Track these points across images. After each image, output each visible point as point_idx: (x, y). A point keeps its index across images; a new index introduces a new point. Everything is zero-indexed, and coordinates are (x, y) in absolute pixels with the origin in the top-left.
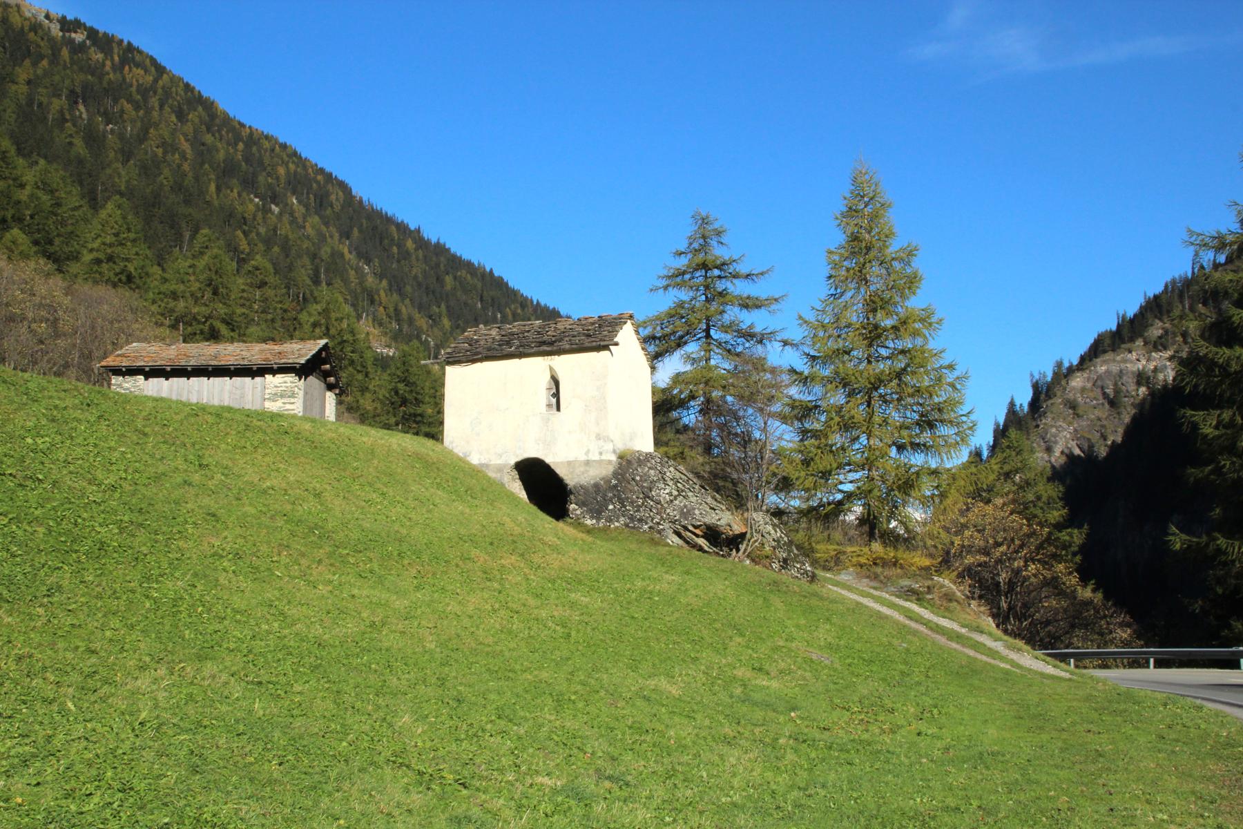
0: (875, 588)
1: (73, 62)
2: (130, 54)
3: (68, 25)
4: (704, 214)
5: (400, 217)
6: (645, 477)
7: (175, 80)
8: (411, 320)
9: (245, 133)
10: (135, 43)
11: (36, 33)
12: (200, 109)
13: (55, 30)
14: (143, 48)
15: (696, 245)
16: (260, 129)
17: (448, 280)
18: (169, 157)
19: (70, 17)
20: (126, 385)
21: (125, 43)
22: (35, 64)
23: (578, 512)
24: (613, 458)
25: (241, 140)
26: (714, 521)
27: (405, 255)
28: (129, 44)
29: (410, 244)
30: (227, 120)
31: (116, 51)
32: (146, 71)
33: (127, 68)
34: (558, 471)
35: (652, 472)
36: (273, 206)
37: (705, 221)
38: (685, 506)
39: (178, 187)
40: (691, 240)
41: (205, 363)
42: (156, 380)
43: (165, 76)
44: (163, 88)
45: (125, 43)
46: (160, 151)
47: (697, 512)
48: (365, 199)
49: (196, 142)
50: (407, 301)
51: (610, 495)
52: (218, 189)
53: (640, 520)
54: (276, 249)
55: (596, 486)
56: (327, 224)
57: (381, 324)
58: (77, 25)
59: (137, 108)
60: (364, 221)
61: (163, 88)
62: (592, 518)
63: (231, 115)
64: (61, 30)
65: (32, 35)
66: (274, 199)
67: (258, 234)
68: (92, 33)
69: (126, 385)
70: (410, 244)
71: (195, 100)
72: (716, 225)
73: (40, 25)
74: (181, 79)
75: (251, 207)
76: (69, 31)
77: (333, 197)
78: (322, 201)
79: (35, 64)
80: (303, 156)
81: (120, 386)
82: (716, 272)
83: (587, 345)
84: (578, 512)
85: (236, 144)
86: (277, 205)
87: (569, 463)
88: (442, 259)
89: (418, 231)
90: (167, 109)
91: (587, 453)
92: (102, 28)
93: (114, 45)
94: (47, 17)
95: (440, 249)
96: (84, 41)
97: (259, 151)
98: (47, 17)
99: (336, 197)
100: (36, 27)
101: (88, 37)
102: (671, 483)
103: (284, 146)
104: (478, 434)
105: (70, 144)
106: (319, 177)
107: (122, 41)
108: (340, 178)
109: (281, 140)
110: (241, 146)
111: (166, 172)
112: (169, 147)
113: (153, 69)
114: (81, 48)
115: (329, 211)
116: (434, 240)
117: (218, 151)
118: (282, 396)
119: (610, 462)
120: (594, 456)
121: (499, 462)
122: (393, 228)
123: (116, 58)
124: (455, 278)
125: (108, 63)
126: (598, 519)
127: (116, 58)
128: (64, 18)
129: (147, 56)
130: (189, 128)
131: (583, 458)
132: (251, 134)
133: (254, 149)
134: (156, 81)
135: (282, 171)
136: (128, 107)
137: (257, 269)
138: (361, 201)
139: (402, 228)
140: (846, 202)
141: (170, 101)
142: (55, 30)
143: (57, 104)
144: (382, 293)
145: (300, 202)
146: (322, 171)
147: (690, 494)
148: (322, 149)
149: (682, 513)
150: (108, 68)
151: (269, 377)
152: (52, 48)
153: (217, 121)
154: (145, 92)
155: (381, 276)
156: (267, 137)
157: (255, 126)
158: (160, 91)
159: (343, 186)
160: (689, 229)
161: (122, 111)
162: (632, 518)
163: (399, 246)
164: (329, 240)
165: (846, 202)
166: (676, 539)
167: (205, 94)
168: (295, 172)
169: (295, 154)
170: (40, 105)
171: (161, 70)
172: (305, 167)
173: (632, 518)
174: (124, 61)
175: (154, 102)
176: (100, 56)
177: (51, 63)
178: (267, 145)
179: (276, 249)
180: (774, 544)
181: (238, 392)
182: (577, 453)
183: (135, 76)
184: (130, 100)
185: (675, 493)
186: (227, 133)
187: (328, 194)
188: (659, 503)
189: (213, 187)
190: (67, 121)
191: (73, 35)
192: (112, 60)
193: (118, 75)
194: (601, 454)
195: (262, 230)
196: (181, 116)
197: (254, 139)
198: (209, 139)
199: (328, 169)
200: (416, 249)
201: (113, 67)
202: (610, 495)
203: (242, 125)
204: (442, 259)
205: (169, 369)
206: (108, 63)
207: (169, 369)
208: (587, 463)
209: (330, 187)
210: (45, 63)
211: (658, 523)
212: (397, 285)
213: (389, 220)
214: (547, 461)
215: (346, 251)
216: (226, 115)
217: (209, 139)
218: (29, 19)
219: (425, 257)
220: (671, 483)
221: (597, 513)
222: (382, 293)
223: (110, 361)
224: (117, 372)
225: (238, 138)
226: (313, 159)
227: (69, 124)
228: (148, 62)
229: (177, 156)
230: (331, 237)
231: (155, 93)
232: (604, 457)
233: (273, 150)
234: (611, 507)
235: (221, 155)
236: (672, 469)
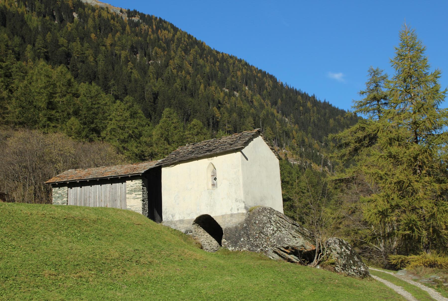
0: (415, 280)
1: (132, 32)
2: (161, 24)
3: (131, 14)
4: (375, 69)
5: (303, 91)
6: (261, 221)
7: (184, 34)
8: (310, 146)
9: (220, 56)
10: (163, 18)
11: (114, 20)
12: (196, 47)
13: (125, 17)
14: (167, 20)
15: (372, 87)
16: (228, 53)
17: (331, 121)
18: (179, 73)
19: (132, 10)
20: (59, 192)
21: (158, 19)
22: (114, 36)
23: (226, 243)
24: (245, 211)
25: (218, 60)
26: (294, 244)
27: (307, 110)
28: (160, 19)
29: (309, 104)
30: (210, 51)
31: (154, 23)
32: (169, 31)
33: (160, 31)
34: (217, 221)
35: (265, 218)
36: (235, 93)
37: (375, 73)
38: (280, 236)
39: (184, 88)
40: (369, 84)
41: (95, 177)
42: (86, 187)
43: (178, 33)
44: (178, 39)
45: (158, 19)
46: (175, 71)
47: (286, 239)
48: (284, 83)
49: (194, 64)
50: (310, 135)
51: (242, 232)
52: (205, 87)
53: (257, 246)
54: (235, 115)
55: (236, 228)
56: (264, 99)
57: (294, 149)
58: (135, 13)
59: (164, 50)
60: (284, 95)
61: (178, 39)
62: (232, 246)
63: (212, 48)
64: (128, 17)
65: (112, 22)
66: (236, 89)
67: (226, 108)
68: (142, 16)
69: (59, 192)
70: (309, 104)
71: (194, 42)
72: (383, 74)
73: (118, 16)
74: (186, 33)
75: (222, 94)
76: (132, 16)
77: (267, 84)
78: (261, 87)
79: (114, 36)
80: (250, 64)
81: (56, 193)
82: (383, 101)
83: (228, 149)
84: (226, 243)
85: (215, 63)
86: (237, 92)
87: (223, 216)
88: (327, 111)
89: (314, 97)
90: (179, 49)
91: (231, 210)
92: (146, 13)
93: (153, 21)
94: (121, 11)
95: (326, 105)
96: (139, 21)
97: (227, 65)
98: (121, 11)
99: (268, 84)
100: (115, 17)
101: (141, 19)
102: (273, 224)
103: (240, 61)
104: (178, 204)
105: (131, 72)
106: (259, 75)
107: (156, 18)
108: (270, 73)
109: (239, 58)
110: (218, 63)
111: (178, 81)
112: (180, 68)
113: (172, 30)
114: (137, 24)
115: (265, 92)
116: (322, 101)
117: (205, 67)
118: (135, 191)
119: (243, 214)
120: (235, 212)
121: (189, 218)
122: (299, 97)
123: (154, 27)
124: (335, 120)
125: (150, 30)
126: (235, 246)
127: (154, 27)
128: (129, 10)
129: (169, 23)
130: (191, 57)
131: (229, 213)
132: (223, 56)
133: (225, 64)
134: (174, 36)
135: (239, 73)
136: (159, 51)
137: (195, 126)
138: (282, 85)
139: (305, 96)
140: (397, 51)
141: (181, 45)
142: (125, 17)
143: (124, 54)
144: (294, 132)
145: (250, 89)
146: (260, 71)
147: (283, 229)
148: (260, 60)
149: (278, 240)
150: (150, 33)
151: (128, 182)
152: (122, 26)
153: (205, 52)
154: (168, 42)
155: (296, 123)
156: (231, 57)
157: (225, 52)
158: (176, 40)
159: (271, 77)
160: (367, 78)
161: (156, 53)
162: (252, 245)
163: (303, 106)
164: (266, 107)
165: (397, 51)
166: (276, 256)
167: (198, 39)
168: (247, 73)
169: (246, 64)
170: (116, 55)
171: (176, 30)
172: (251, 71)
173: (252, 245)
174: (158, 28)
175: (173, 46)
176: (147, 27)
177: (122, 33)
178: (231, 61)
179: (235, 115)
180: (337, 255)
181: (114, 190)
182: (227, 209)
183: (164, 34)
184: (160, 47)
185: (275, 229)
186: (211, 57)
187: (264, 83)
188: (267, 235)
189: (202, 86)
190: (129, 61)
191: (133, 18)
192: (152, 29)
193: (155, 35)
194: (238, 210)
195: (228, 106)
196: (186, 51)
197: (223, 60)
198: (201, 61)
199: (263, 70)
200: (313, 107)
201: (153, 32)
202: (242, 232)
203: (218, 52)
204: (327, 111)
205: (78, 181)
206: (150, 30)
207: (78, 181)
208: (232, 215)
209: (265, 79)
210: (118, 34)
211: (266, 247)
212: (303, 126)
213: (297, 93)
214: (212, 216)
215: (275, 112)
216: (209, 48)
217: (201, 61)
218: (112, 14)
219: (317, 110)
220: (273, 224)
221: (235, 244)
222: (294, 132)
223: (54, 180)
224: (54, 185)
225: (216, 59)
226: (256, 66)
227: (130, 63)
228: (169, 27)
229: (183, 72)
230: (267, 105)
231: (174, 41)
232: (240, 212)
233: (234, 64)
234: (242, 239)
235: (207, 69)
236: (275, 216)
